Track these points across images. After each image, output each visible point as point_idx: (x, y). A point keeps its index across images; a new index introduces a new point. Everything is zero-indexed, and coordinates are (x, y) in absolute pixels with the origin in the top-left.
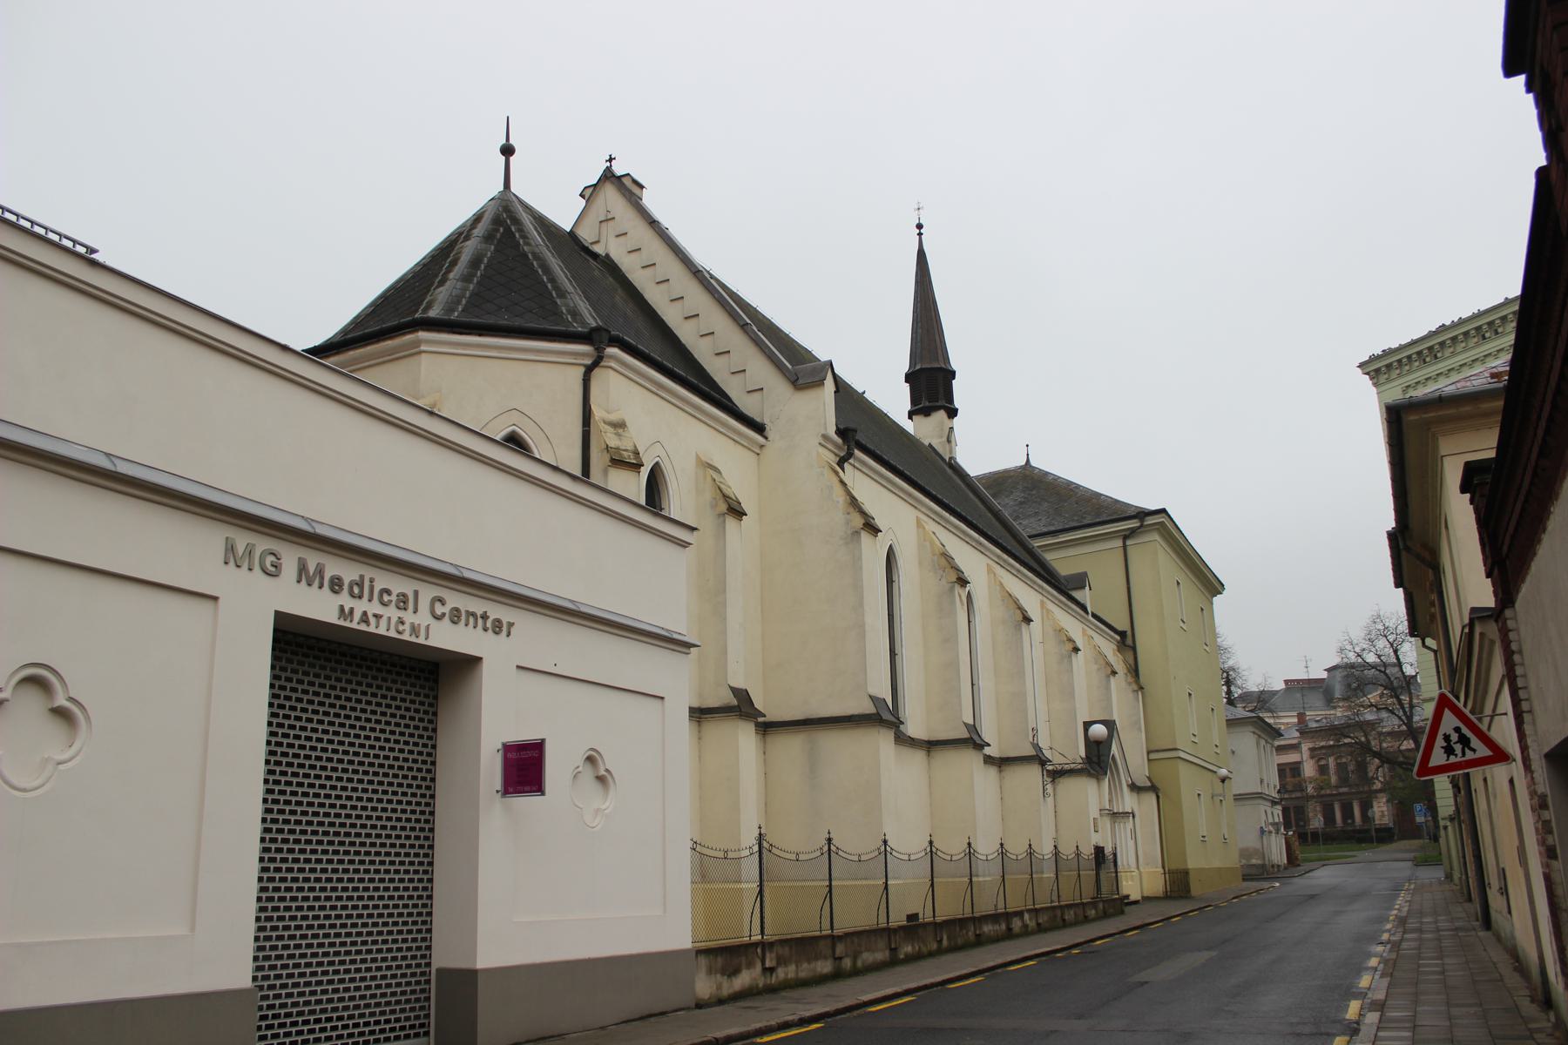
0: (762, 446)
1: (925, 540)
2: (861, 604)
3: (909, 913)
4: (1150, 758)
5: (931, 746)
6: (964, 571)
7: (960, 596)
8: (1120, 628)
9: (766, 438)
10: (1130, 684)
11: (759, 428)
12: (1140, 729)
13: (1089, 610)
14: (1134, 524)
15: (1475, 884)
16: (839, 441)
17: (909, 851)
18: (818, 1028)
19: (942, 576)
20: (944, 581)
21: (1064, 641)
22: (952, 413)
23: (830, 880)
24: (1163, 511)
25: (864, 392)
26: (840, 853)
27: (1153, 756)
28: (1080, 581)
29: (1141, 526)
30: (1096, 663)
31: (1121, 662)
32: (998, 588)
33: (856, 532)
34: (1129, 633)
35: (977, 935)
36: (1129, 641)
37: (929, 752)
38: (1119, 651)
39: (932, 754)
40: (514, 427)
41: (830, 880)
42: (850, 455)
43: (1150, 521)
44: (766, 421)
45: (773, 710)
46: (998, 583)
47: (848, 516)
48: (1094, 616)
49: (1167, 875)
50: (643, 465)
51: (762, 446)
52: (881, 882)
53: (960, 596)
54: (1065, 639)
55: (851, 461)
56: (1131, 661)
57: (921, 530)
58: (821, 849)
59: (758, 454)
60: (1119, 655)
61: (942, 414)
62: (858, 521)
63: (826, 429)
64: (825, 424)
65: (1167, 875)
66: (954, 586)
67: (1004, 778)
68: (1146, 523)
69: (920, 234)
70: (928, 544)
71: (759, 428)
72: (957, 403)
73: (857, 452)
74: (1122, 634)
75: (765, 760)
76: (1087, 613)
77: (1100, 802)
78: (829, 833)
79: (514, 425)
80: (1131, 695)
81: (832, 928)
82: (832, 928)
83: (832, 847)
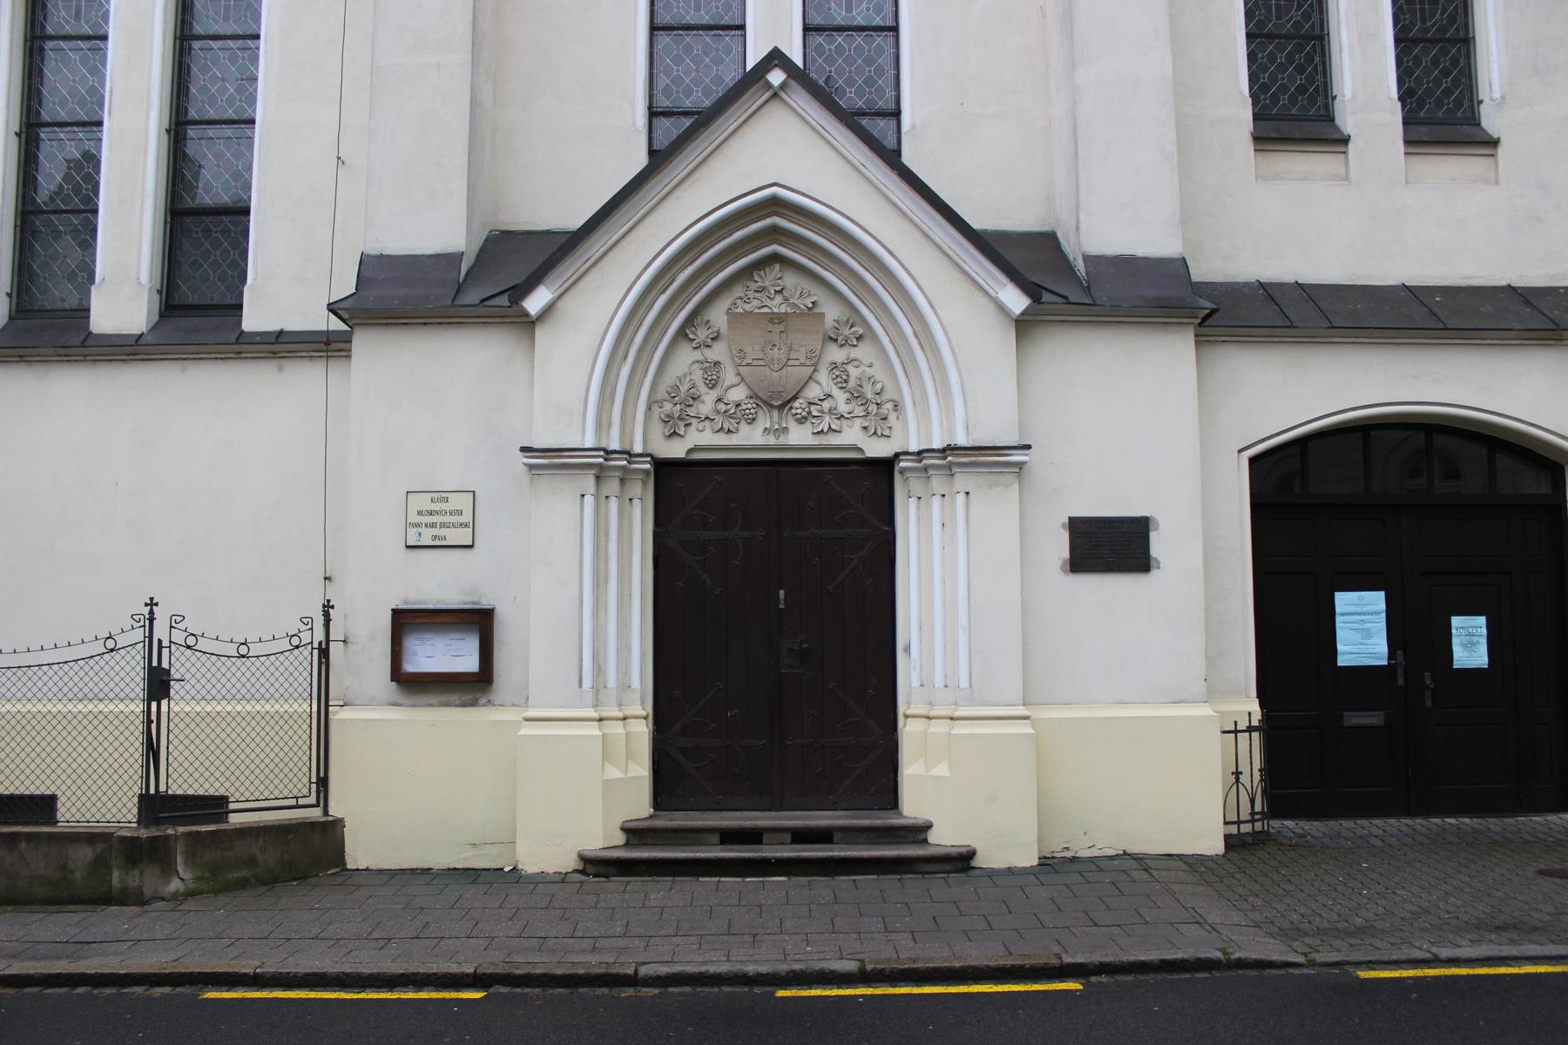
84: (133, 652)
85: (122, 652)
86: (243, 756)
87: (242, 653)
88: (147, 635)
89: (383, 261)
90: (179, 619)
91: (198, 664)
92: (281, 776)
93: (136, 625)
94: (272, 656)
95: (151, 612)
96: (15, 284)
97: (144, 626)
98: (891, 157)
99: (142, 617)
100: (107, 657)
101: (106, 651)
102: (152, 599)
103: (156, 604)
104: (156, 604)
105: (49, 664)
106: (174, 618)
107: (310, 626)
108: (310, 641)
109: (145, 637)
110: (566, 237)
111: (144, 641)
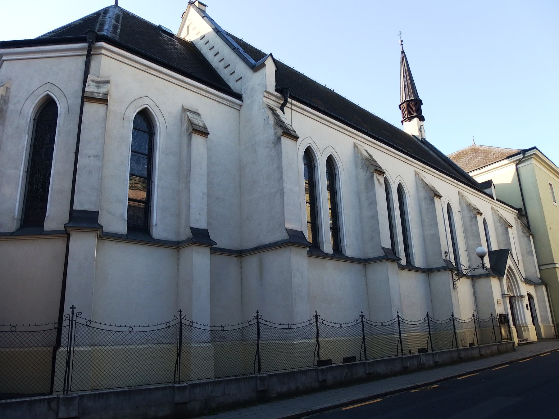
0: (241, 106)
1: (358, 154)
2: (282, 178)
3: (420, 348)
4: (540, 269)
5: (365, 262)
6: (479, 209)
7: (378, 180)
8: (518, 207)
9: (242, 101)
10: (525, 233)
11: (239, 97)
12: (532, 255)
13: (495, 197)
14: (520, 156)
15: (74, 52)
16: (279, 95)
17: (464, 319)
18: (507, 366)
19: (367, 170)
20: (368, 173)
21: (472, 210)
22: (422, 119)
23: (318, 337)
24: (535, 148)
25: (326, 86)
26: (325, 323)
27: (542, 268)
28: (488, 184)
29: (524, 157)
30: (500, 223)
31: (520, 224)
32: (421, 182)
33: (279, 138)
34: (523, 209)
35: (435, 362)
36: (524, 213)
37: (535, 286)
38: (518, 219)
39: (367, 266)
40: (48, 92)
41: (318, 337)
42: (286, 102)
43: (528, 154)
44: (243, 93)
45: (222, 242)
46: (421, 180)
47: (276, 130)
48: (497, 200)
49: (556, 327)
50: (209, 134)
51: (241, 106)
52: (314, 340)
53: (378, 180)
54: (473, 208)
55: (288, 105)
56: (526, 222)
57: (356, 149)
58: (450, 319)
59: (239, 110)
60: (518, 220)
61: (416, 120)
62: (280, 131)
63: (266, 88)
64: (266, 85)
65: (556, 327)
66: (373, 175)
67: (430, 279)
68: (525, 156)
69: (402, 44)
70: (360, 155)
71: (239, 97)
72: (424, 114)
73: (289, 100)
74: (519, 210)
75: (241, 272)
76: (494, 199)
77: (502, 291)
78: (398, 313)
79: (48, 91)
80: (526, 239)
81: (402, 354)
82: (402, 354)
83: (400, 319)
84: (255, 325)
85: (253, 325)
86: (109, 360)
87: (12, 330)
88: (179, 321)
89: (420, 349)
90: (80, 314)
91: (188, 329)
92: (122, 361)
93: (255, 318)
94: (45, 331)
95: (73, 311)
96: (393, 239)
97: (178, 319)
98: (429, 282)
99: (69, 316)
100: (249, 327)
101: (167, 327)
102: (73, 306)
103: (75, 308)
104: (75, 308)
105: (149, 331)
106: (78, 313)
107: (177, 318)
108: (68, 325)
109: (178, 322)
110: (419, 99)
111: (178, 323)
